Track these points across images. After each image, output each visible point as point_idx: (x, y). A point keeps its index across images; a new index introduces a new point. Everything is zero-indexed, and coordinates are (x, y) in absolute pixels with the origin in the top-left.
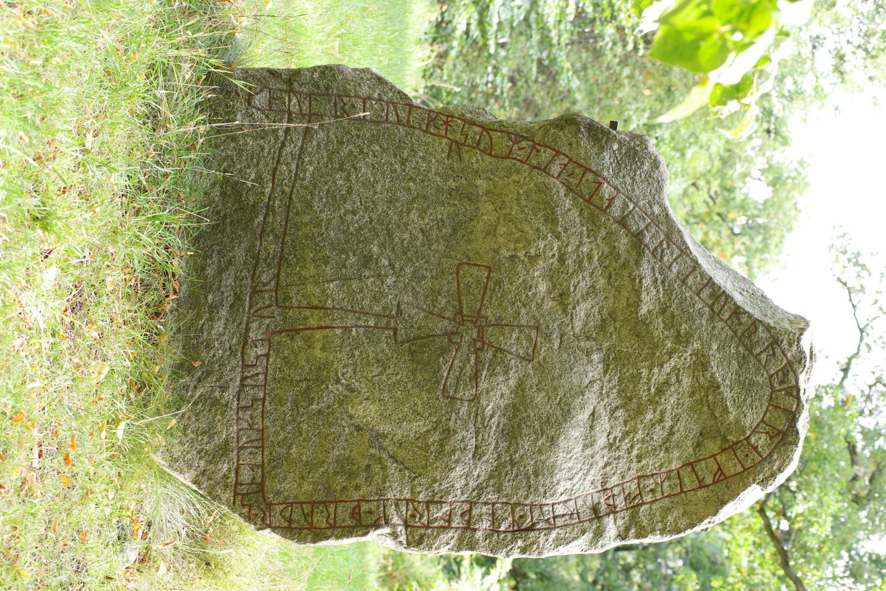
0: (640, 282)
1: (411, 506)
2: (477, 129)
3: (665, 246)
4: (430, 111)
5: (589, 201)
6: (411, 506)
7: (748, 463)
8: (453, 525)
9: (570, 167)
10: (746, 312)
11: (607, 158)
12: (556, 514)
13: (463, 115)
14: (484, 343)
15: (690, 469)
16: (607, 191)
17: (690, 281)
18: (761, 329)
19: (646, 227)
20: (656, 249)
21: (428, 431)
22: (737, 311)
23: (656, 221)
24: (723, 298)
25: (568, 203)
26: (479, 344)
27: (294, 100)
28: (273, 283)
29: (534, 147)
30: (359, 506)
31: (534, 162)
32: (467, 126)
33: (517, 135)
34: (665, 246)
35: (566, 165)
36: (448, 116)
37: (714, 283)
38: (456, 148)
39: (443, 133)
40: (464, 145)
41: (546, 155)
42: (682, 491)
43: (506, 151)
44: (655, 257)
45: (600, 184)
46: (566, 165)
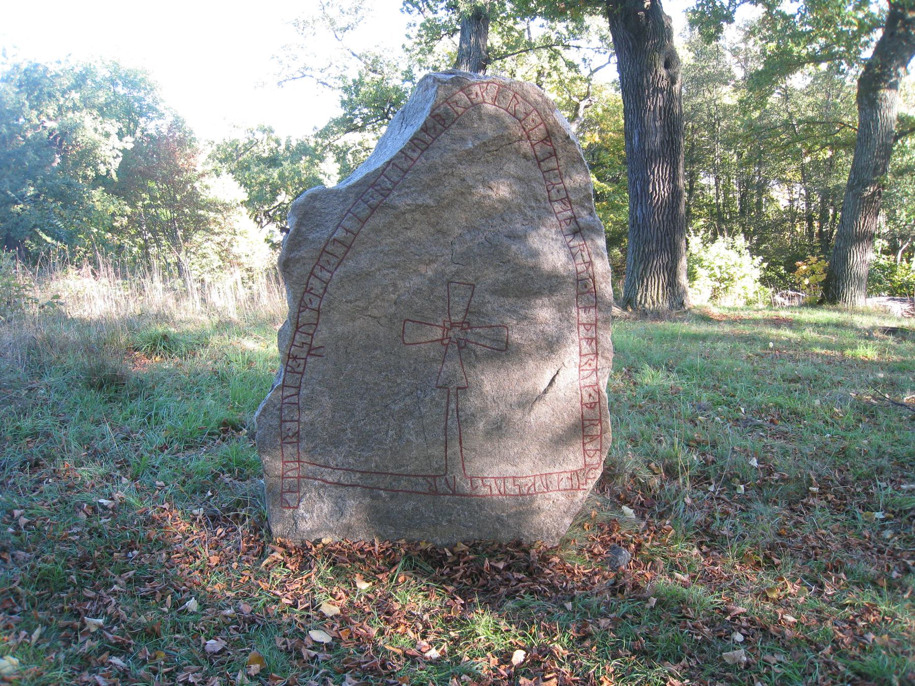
0: (409, 205)
1: (584, 368)
2: (297, 337)
3: (379, 188)
4: (286, 371)
5: (349, 247)
6: (584, 368)
7: (538, 120)
8: (594, 336)
9: (322, 263)
10: (425, 123)
11: (314, 236)
12: (345, 249)
13: (287, 346)
14: (463, 322)
15: (542, 163)
16: (340, 234)
17: (405, 166)
18: (437, 111)
19: (366, 202)
20: (382, 194)
21: (203, 300)
22: (425, 129)
23: (359, 196)
24: (415, 141)
25: (351, 263)
26: (465, 326)
27: (290, 474)
28: (429, 479)
29: (309, 292)
30: (586, 404)
31: (321, 291)
32: (295, 343)
33: (300, 306)
34: (379, 188)
35: (322, 267)
36: (289, 358)
37: (404, 149)
38: (312, 351)
39: (302, 361)
40: (311, 345)
41: (314, 282)
42: (558, 169)
43: (315, 314)
44: (388, 195)
45: (335, 240)
46: (322, 267)
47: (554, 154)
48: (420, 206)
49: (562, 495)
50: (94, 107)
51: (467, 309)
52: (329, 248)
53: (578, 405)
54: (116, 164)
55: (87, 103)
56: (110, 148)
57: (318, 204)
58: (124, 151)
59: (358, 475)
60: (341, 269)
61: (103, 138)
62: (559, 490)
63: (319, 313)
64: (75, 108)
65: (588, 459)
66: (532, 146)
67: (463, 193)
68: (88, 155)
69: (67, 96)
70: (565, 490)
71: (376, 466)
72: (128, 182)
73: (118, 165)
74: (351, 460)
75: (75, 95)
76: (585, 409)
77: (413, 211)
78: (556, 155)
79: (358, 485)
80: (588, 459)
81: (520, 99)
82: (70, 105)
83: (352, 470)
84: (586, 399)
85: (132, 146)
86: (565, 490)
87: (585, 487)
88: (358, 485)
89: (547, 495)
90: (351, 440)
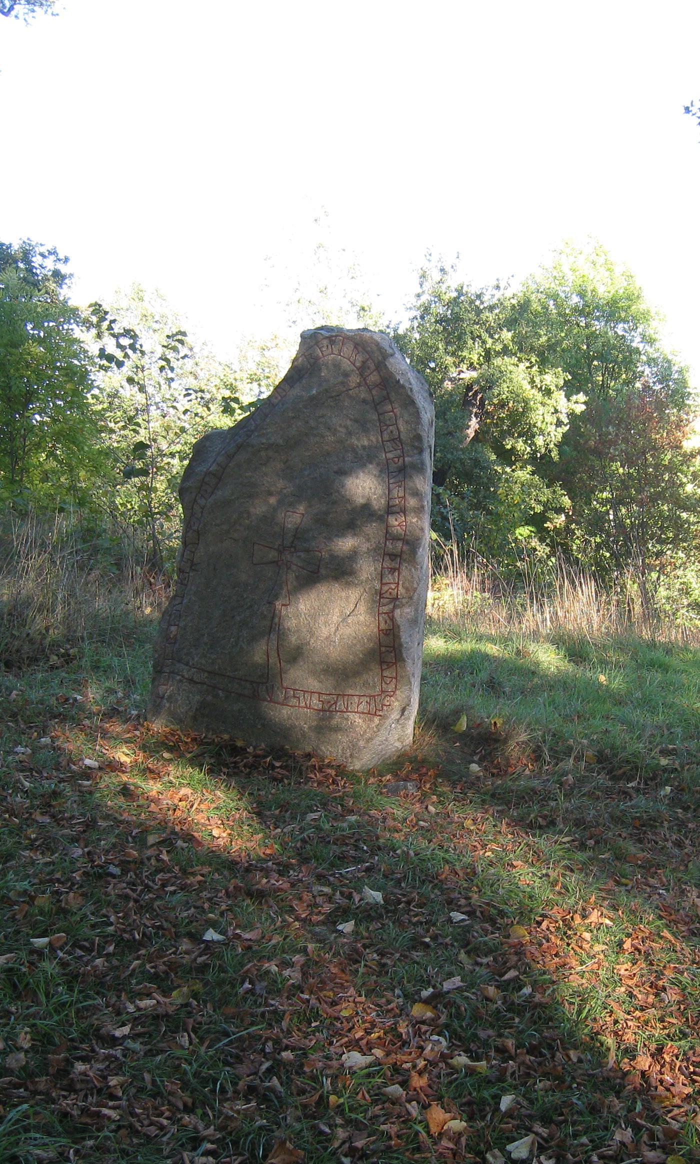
25: (220, 493)
47: (387, 398)
48: (272, 445)
49: (360, 718)
50: (532, 349)
51: (295, 536)
52: (207, 479)
53: (376, 630)
54: (557, 434)
55: (522, 346)
56: (552, 409)
57: (208, 444)
58: (572, 415)
59: (206, 675)
60: (213, 497)
61: (539, 396)
62: (357, 712)
63: (199, 535)
64: (505, 351)
65: (384, 686)
66: (370, 390)
67: (306, 434)
68: (519, 421)
69: (496, 336)
70: (363, 713)
71: (219, 668)
72: (572, 465)
73: (559, 437)
74: (203, 662)
75: (507, 335)
76: (382, 635)
77: (267, 449)
78: (389, 398)
79: (205, 684)
80: (384, 686)
81: (360, 349)
82: (499, 347)
83: (202, 670)
84: (383, 626)
85: (583, 407)
86: (363, 713)
87: (380, 713)
88: (205, 684)
89: (345, 715)
90: (206, 644)
